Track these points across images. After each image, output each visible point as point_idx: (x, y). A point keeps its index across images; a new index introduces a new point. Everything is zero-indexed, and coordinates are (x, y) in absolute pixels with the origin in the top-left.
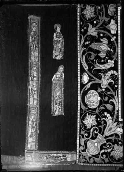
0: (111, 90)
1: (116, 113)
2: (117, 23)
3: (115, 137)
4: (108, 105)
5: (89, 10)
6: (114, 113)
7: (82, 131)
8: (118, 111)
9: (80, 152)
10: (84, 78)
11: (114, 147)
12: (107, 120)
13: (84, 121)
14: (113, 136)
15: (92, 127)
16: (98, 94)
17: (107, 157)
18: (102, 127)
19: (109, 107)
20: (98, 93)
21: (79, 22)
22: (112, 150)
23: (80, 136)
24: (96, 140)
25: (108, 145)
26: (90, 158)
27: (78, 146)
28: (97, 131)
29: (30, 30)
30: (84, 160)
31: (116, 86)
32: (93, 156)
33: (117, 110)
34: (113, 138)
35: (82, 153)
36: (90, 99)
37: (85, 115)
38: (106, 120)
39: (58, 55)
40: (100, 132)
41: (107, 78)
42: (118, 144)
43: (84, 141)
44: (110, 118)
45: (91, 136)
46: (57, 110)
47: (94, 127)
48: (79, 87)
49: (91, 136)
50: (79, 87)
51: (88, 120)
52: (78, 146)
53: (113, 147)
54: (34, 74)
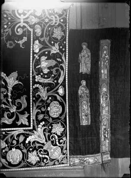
0: (7, 137)
1: (26, 132)
2: (33, 51)
3: (36, 146)
4: (20, 140)
5: (58, 35)
6: (26, 134)
7: (42, 165)
8: (24, 130)
9: (60, 164)
10: (62, 91)
11: (54, 132)
12: (32, 141)
13: (34, 164)
14: (21, 162)
15: (38, 156)
16: (10, 151)
17: (62, 139)
18: (37, 145)
19: (21, 139)
20: (9, 151)
21: (67, 43)
22: (56, 134)
24: (49, 150)
25: (52, 139)
26: (64, 154)
28: (42, 151)
30: (65, 159)
31: (34, 99)
32: (62, 152)
33: (23, 131)
34: (47, 134)
35: (60, 162)
36: (15, 159)
37: (30, 163)
39: (85, 68)
40: (42, 148)
41: (42, 91)
42: (51, 130)
44: (30, 137)
45: (46, 156)
47: (38, 153)
48: (67, 97)
49: (46, 156)
50: (67, 97)
51: (56, 128)
53: (54, 134)
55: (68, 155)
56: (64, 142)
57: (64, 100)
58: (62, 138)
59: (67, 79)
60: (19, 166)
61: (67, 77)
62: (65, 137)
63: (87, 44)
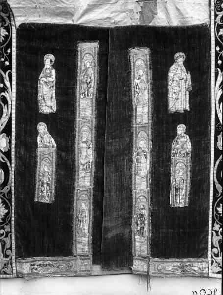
7: (215, 224)
9: (212, 257)
23: (212, 233)
26: (7, 256)
27: (210, 246)
29: (81, 55)
38: (6, 96)
39: (179, 99)
43: (219, 241)
46: (180, 200)
52: (210, 246)
54: (143, 143)
55: (14, 261)
56: (7, 233)
57: (8, 159)
58: (4, 226)
59: (13, 126)
60: (217, 182)
61: (13, 122)
62: (9, 226)
63: (184, 54)
